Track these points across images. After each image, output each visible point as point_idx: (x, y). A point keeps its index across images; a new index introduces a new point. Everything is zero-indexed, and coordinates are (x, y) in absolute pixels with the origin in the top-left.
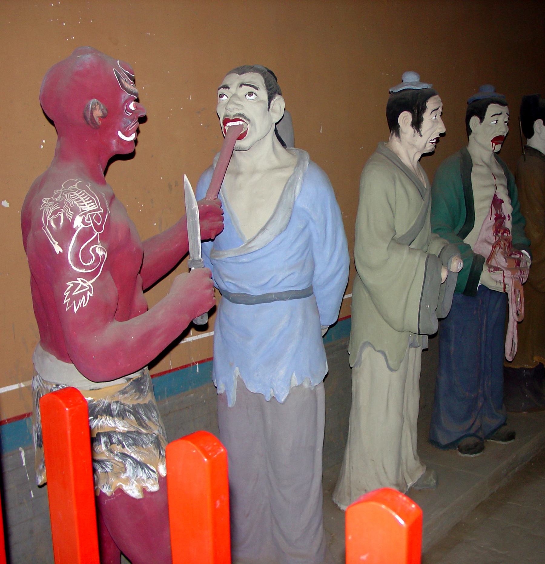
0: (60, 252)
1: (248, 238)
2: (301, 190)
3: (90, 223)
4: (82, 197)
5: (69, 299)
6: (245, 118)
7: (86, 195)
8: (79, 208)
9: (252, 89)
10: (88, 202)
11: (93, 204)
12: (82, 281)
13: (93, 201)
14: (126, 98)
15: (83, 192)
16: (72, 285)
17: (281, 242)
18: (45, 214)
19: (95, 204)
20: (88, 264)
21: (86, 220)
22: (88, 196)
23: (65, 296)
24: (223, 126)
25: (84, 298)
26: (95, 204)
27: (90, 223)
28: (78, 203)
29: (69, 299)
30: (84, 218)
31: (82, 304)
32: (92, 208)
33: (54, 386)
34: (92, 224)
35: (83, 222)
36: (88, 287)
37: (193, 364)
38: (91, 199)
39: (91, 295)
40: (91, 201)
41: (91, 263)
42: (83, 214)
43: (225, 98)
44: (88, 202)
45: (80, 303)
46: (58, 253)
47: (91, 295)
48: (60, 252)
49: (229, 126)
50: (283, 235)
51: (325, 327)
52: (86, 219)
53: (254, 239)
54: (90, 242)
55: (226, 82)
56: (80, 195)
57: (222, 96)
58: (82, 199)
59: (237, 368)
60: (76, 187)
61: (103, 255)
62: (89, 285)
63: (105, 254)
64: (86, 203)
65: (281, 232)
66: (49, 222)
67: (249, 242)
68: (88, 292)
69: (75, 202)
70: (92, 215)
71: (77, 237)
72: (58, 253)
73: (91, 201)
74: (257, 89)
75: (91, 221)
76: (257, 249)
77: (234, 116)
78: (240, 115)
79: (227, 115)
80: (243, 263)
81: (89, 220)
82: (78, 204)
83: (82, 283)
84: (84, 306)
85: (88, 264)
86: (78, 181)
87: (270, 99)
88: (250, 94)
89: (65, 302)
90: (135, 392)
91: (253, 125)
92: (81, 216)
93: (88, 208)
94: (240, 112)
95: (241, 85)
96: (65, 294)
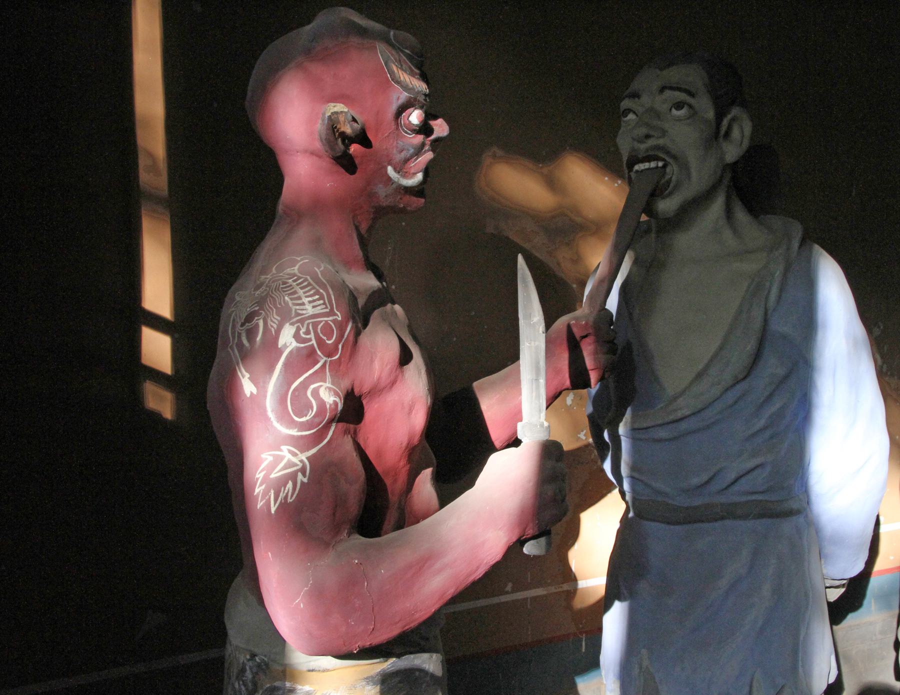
0: (252, 393)
1: (670, 391)
2: (779, 297)
3: (310, 340)
4: (302, 288)
5: (263, 487)
6: (668, 153)
7: (309, 284)
8: (290, 310)
9: (682, 96)
10: (310, 299)
11: (321, 302)
12: (290, 451)
13: (322, 298)
14: (401, 101)
15: (306, 280)
16: (271, 458)
17: (736, 402)
18: (234, 320)
19: (324, 304)
20: (304, 419)
21: (301, 332)
22: (314, 288)
23: (258, 479)
24: (626, 171)
25: (290, 485)
26: (324, 304)
27: (310, 340)
28: (291, 299)
29: (263, 487)
30: (298, 329)
31: (286, 497)
32: (318, 310)
33: (248, 657)
34: (314, 342)
35: (297, 336)
36: (301, 465)
37: (575, 635)
38: (317, 293)
39: (305, 480)
40: (317, 297)
41: (308, 418)
42: (298, 321)
43: (631, 116)
44: (310, 299)
45: (282, 495)
46: (248, 395)
47: (305, 480)
48: (252, 393)
49: (637, 171)
50: (744, 386)
51: (837, 583)
52: (303, 330)
53: (683, 392)
54: (310, 375)
55: (635, 86)
56: (298, 285)
57: (628, 111)
58: (301, 292)
59: (644, 651)
60: (296, 271)
61: (335, 402)
62: (301, 461)
63: (338, 400)
64: (306, 300)
65: (737, 382)
66: (239, 334)
67: (675, 398)
68: (300, 474)
69: (286, 298)
70: (315, 325)
71: (286, 365)
72: (248, 395)
73: (317, 297)
74: (691, 94)
75: (312, 336)
76: (688, 413)
77: (647, 150)
78: (658, 148)
79: (633, 149)
80: (660, 440)
81: (307, 332)
82: (290, 303)
83: (289, 456)
84: (289, 500)
85: (304, 419)
86: (302, 260)
87: (720, 116)
88: (679, 106)
89: (257, 490)
90: (400, 682)
91: (685, 167)
92: (292, 324)
93: (309, 310)
94: (661, 142)
95: (662, 90)
96: (257, 476)
